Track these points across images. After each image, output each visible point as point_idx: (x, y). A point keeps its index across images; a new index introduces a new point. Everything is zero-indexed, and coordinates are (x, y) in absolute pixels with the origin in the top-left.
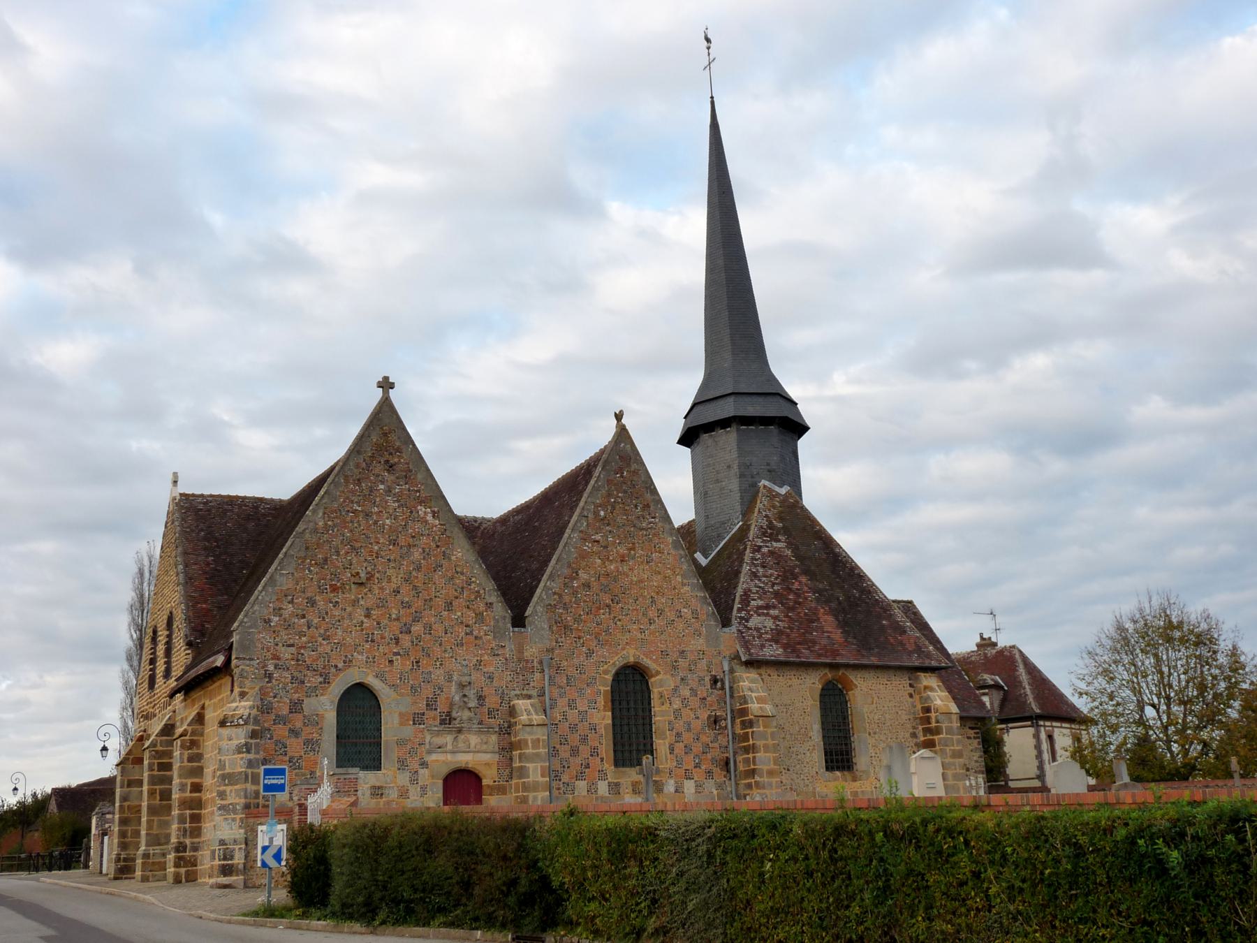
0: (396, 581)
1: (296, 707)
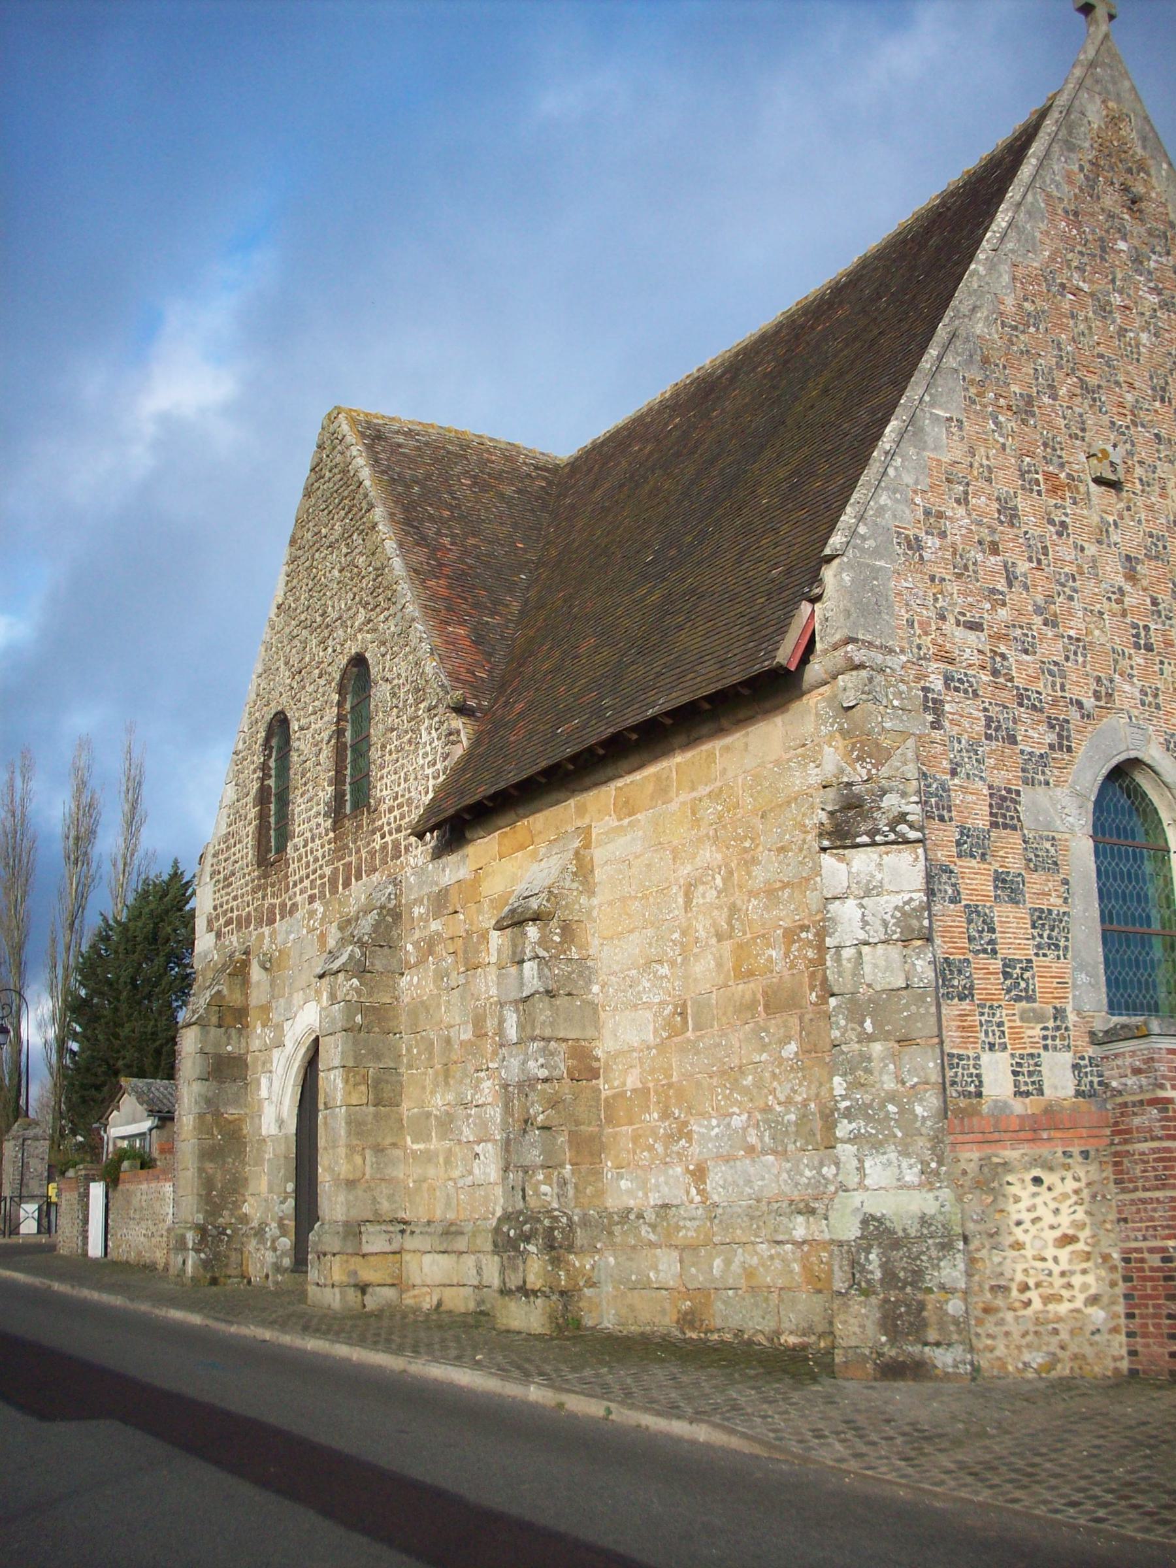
1: (1004, 809)
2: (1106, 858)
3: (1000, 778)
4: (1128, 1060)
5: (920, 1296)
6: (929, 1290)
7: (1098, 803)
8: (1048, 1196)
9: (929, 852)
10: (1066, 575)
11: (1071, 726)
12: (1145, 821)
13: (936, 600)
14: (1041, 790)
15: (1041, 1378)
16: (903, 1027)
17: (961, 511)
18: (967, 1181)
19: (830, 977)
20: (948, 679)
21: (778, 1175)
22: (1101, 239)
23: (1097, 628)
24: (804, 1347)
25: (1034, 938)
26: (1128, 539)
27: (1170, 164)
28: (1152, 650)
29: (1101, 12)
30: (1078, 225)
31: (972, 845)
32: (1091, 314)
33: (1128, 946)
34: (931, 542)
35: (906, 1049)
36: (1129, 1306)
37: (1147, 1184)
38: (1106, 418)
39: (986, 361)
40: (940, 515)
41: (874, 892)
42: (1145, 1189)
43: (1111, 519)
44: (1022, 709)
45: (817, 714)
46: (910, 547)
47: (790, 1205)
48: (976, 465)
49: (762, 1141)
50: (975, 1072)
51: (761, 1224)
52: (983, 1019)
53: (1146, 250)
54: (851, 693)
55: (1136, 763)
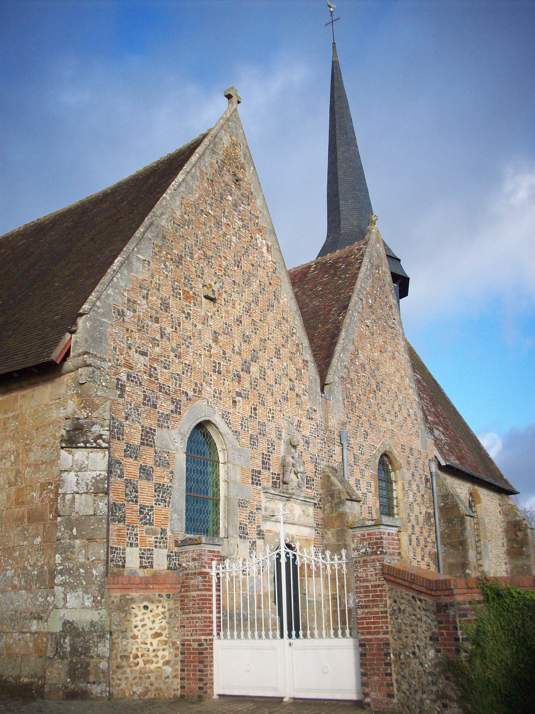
0: (238, 310)
1: (148, 437)
2: (191, 463)
3: (147, 423)
4: (191, 554)
5: (87, 660)
6: (92, 657)
7: (190, 439)
8: (150, 615)
9: (111, 454)
10: (187, 336)
11: (182, 403)
12: (210, 448)
13: (128, 340)
14: (165, 430)
15: (140, 699)
16: (91, 533)
17: (144, 302)
18: (114, 606)
19: (59, 508)
20: (129, 376)
21: (26, 600)
22: (221, 194)
23: (198, 361)
24: (32, 684)
25: (155, 496)
26: (216, 324)
27: (254, 168)
28: (221, 374)
29: (234, 99)
30: (212, 186)
31: (131, 452)
32: (212, 225)
33: (197, 503)
34: (129, 314)
35: (90, 544)
36: (182, 666)
37: (195, 611)
38: (213, 271)
39: (164, 237)
40: (135, 302)
41: (84, 470)
42: (193, 613)
43: (209, 314)
44: (161, 393)
45: (67, 385)
46: (119, 315)
47: (31, 615)
48: (154, 282)
49: (20, 583)
50: (122, 556)
51: (16, 623)
52: (128, 532)
53: (240, 202)
54: (84, 377)
55: (208, 422)
